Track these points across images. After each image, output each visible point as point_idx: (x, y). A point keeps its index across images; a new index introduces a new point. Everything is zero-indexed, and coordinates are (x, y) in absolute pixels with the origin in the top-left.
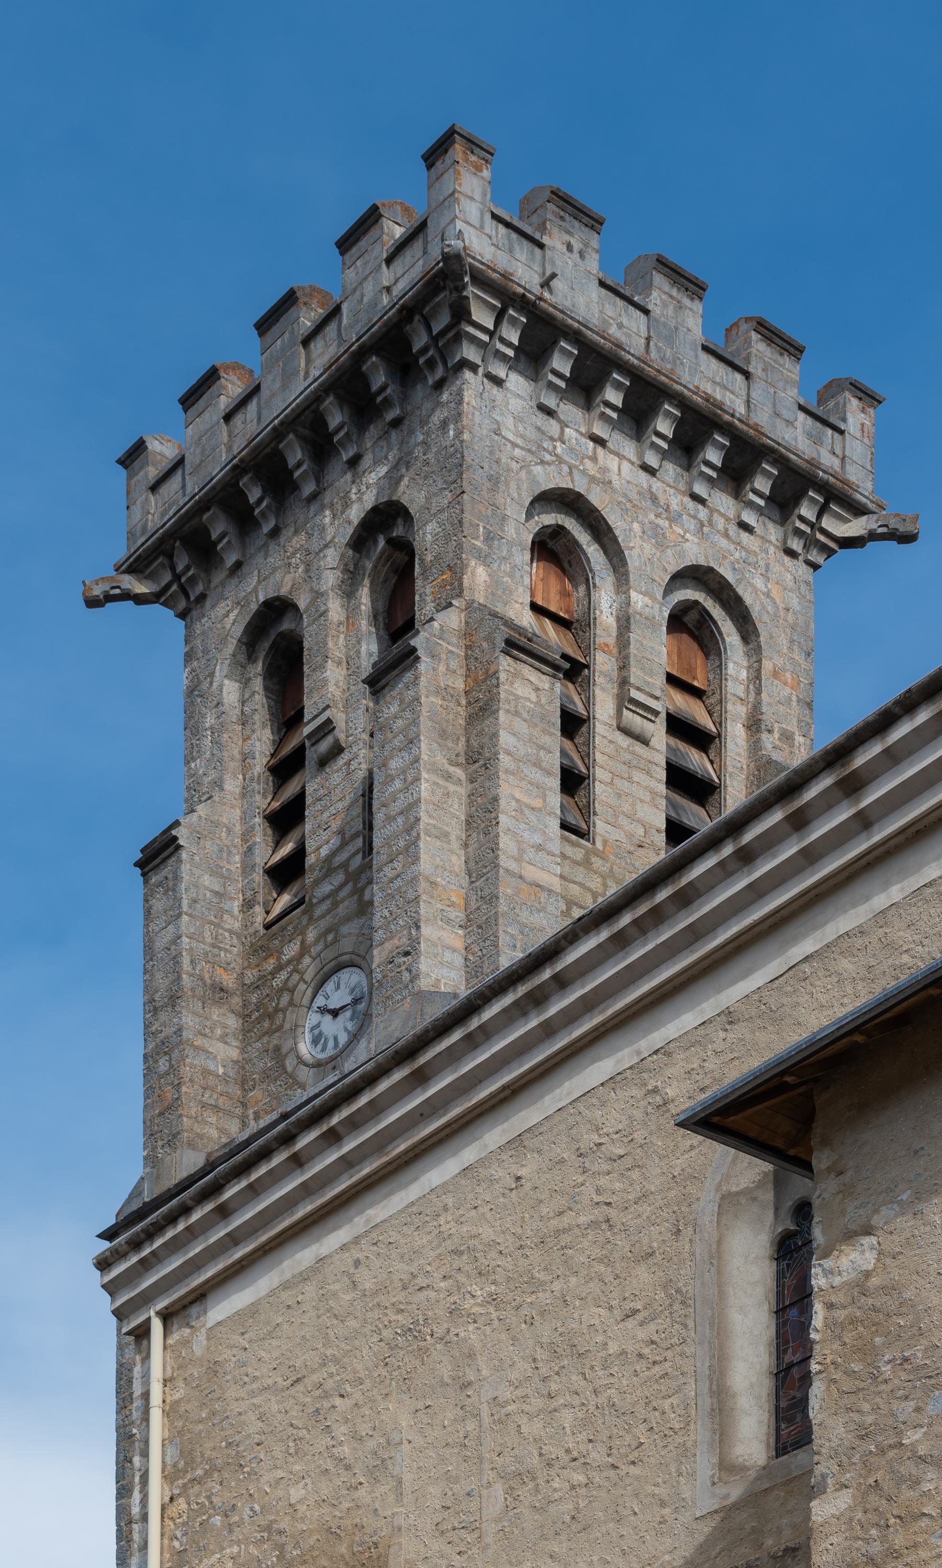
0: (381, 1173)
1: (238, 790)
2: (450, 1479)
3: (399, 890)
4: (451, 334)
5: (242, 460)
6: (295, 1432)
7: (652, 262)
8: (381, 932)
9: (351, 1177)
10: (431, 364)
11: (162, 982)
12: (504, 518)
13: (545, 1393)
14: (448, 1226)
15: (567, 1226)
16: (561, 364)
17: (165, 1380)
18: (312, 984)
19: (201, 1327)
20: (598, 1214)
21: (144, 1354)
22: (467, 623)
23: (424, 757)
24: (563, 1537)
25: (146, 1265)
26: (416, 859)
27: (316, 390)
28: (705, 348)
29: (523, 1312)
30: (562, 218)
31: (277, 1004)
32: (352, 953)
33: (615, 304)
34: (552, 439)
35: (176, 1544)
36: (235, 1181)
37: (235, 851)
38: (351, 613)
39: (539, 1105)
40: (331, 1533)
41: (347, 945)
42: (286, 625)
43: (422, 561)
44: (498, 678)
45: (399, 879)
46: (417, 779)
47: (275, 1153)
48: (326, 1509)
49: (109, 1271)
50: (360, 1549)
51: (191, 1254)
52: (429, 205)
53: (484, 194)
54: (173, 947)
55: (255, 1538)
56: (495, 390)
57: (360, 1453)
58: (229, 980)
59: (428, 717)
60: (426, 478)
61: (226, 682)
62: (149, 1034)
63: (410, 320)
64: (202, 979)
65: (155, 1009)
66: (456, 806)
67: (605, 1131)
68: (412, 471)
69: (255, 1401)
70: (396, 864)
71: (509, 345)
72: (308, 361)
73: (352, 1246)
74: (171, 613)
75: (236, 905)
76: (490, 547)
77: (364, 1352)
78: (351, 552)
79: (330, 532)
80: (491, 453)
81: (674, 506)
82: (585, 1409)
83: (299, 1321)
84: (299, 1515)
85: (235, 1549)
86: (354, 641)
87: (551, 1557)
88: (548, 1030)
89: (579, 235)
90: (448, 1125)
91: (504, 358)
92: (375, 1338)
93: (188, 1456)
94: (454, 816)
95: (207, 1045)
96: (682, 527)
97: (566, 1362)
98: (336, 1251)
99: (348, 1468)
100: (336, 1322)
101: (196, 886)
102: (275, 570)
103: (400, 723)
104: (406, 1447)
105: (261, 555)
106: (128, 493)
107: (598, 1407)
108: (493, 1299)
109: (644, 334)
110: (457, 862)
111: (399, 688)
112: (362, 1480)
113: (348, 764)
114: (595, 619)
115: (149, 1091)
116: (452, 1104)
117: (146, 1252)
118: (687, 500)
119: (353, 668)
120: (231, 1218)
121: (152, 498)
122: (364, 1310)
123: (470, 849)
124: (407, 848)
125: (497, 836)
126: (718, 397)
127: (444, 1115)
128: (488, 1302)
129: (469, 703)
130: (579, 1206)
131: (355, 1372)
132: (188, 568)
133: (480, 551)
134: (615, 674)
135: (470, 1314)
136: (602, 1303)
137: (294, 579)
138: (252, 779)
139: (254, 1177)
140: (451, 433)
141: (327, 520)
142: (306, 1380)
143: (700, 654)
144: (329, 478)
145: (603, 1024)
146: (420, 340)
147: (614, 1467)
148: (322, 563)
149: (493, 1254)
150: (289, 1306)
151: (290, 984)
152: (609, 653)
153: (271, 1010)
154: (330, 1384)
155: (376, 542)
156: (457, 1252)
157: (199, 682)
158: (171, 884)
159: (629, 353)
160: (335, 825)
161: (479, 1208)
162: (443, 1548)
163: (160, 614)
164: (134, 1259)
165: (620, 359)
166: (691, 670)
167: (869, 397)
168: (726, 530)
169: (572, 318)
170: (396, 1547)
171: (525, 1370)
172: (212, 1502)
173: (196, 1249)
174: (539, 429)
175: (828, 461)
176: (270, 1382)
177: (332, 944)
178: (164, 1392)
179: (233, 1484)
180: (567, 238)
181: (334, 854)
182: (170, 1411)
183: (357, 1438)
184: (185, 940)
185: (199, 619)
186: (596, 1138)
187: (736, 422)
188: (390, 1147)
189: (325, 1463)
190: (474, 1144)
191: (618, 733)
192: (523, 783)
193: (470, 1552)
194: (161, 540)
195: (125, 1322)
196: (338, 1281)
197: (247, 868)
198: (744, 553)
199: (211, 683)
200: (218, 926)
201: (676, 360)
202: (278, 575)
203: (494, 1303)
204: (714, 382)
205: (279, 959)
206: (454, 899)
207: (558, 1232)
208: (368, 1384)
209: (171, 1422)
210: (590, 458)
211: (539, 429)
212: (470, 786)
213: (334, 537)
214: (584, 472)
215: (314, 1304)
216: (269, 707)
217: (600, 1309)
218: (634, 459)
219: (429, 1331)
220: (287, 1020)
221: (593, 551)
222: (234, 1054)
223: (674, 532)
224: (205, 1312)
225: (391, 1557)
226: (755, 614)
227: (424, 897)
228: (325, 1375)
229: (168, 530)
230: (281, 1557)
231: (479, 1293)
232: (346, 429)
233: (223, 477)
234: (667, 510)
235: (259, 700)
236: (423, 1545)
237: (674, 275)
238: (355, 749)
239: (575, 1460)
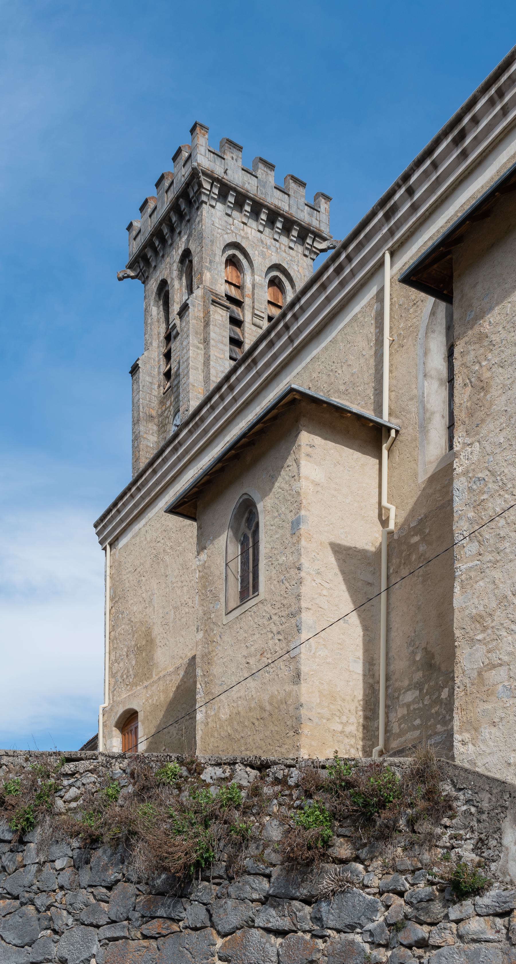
1: (157, 346)
4: (198, 192)
7: (258, 159)
10: (195, 201)
12: (215, 255)
16: (231, 199)
23: (191, 342)
26: (188, 378)
28: (275, 188)
30: (230, 148)
33: (247, 176)
34: (230, 225)
46: (189, 349)
56: (212, 210)
58: (154, 413)
61: (153, 307)
63: (188, 187)
64: (146, 414)
71: (215, 194)
74: (140, 282)
76: (211, 265)
78: (180, 265)
80: (211, 232)
81: (269, 244)
89: (236, 153)
91: (214, 199)
104: (155, 595)
109: (256, 185)
118: (273, 240)
126: (280, 205)
132: (143, 267)
133: (208, 267)
143: (280, 293)
146: (191, 194)
152: (249, 297)
163: (138, 282)
165: (248, 195)
166: (277, 299)
167: (327, 198)
174: (226, 222)
175: (315, 223)
180: (232, 155)
184: (141, 400)
194: (136, 258)
197: (159, 373)
200: (150, 394)
201: (266, 194)
204: (279, 199)
211: (226, 222)
214: (240, 235)
218: (256, 228)
221: (244, 262)
222: (156, 439)
226: (294, 279)
227: (191, 391)
234: (266, 245)
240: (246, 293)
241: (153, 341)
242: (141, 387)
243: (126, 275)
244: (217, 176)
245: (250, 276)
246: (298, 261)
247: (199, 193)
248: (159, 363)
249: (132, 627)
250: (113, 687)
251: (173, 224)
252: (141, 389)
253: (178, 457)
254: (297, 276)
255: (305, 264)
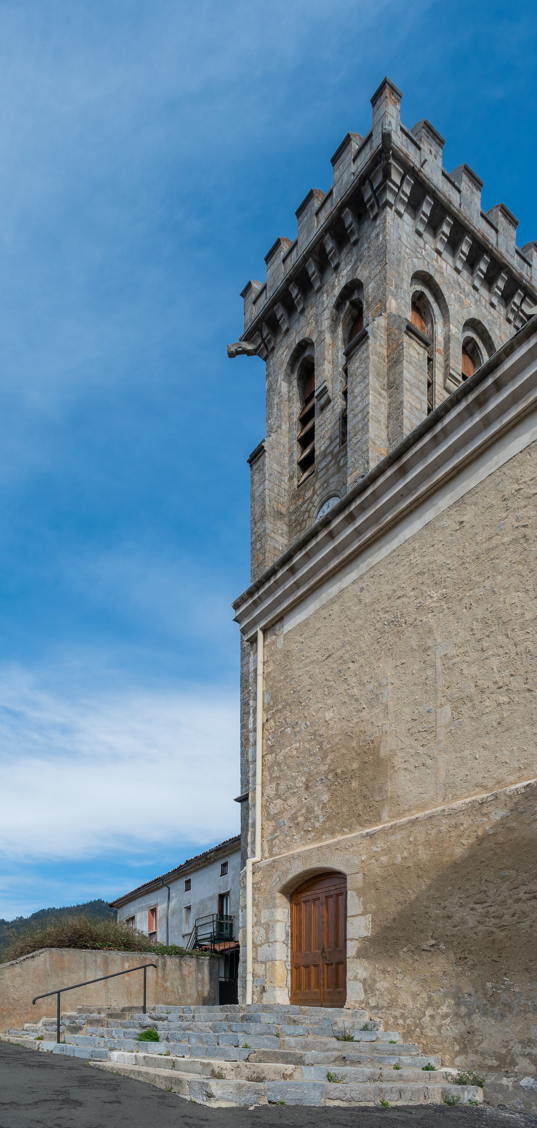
0: (376, 537)
1: (287, 430)
2: (416, 703)
3: (359, 448)
5: (290, 276)
6: (328, 683)
8: (351, 469)
9: (360, 540)
10: (372, 207)
11: (258, 510)
13: (479, 648)
14: (415, 560)
15: (495, 545)
17: (264, 662)
18: (318, 507)
19: (281, 634)
20: (517, 534)
21: (254, 651)
22: (388, 324)
23: (371, 383)
24: (492, 735)
25: (256, 604)
27: (322, 231)
29: (464, 602)
30: (428, 137)
31: (303, 519)
32: (335, 490)
34: (421, 247)
35: (269, 742)
36: (299, 552)
37: (286, 455)
38: (334, 339)
39: (475, 475)
40: (348, 735)
41: (332, 487)
42: (307, 354)
43: (367, 302)
44: (403, 345)
45: (359, 443)
46: (368, 394)
47: (320, 533)
48: (345, 723)
49: (239, 609)
50: (364, 744)
51: (277, 596)
52: (373, 124)
53: (398, 117)
54: (262, 495)
55: (308, 739)
57: (364, 692)
58: (284, 510)
59: (373, 365)
60: (369, 263)
61: (283, 382)
62: (253, 533)
64: (273, 508)
65: (255, 522)
66: (383, 409)
67: (523, 480)
68: (362, 263)
69: (307, 669)
70: (358, 436)
71: (406, 195)
72: (318, 222)
73: (359, 580)
75: (286, 478)
76: (397, 291)
77: (366, 637)
78: (335, 311)
79: (326, 303)
81: (467, 290)
82: (507, 656)
83: (330, 625)
84: (330, 726)
85: (298, 745)
86: (335, 352)
87: (483, 747)
88: (486, 423)
89: (435, 148)
90: (417, 499)
92: (372, 628)
93: (274, 698)
94: (382, 413)
95: (275, 537)
96: (469, 300)
97: (494, 629)
98: (350, 585)
99: (357, 700)
100: (350, 623)
101: (271, 468)
102: (302, 328)
103: (360, 370)
104: (390, 687)
105: (297, 323)
106: (245, 308)
107: (517, 654)
108: (445, 597)
109: (459, 202)
110: (384, 435)
111: (360, 354)
112: (364, 706)
113: (333, 407)
114: (435, 337)
115: (253, 557)
116: (421, 485)
117: (256, 597)
118: (471, 288)
119: (335, 364)
120: (296, 573)
121: (254, 308)
122: (366, 614)
123: (389, 429)
124: (363, 427)
125: (402, 420)
127: (415, 493)
128: (441, 599)
129: (389, 361)
130: (504, 532)
131: (360, 648)
132: (268, 335)
133: (393, 292)
134: (443, 364)
135: (429, 608)
136: (519, 589)
137: (311, 329)
138: (293, 424)
139: (308, 548)
140: (381, 238)
141: (325, 298)
142: (334, 655)
143: (472, 366)
144: (325, 279)
145: (524, 410)
146: (368, 194)
147: (529, 690)
148: (323, 318)
149: (445, 571)
150: (325, 618)
151: (308, 509)
153: (300, 521)
154: (347, 656)
155: (345, 304)
156: (421, 573)
157: (272, 385)
158: (261, 468)
159: (454, 206)
160: (327, 436)
161: (435, 546)
162: (412, 743)
164: (250, 601)
165: (450, 209)
168: (486, 305)
169: (432, 184)
170: (384, 742)
171: (466, 636)
172: (286, 721)
173: (279, 592)
176: (315, 658)
177: (326, 488)
178: (264, 668)
179: (296, 712)
180: (430, 147)
181: (327, 448)
182: (267, 677)
183: (362, 684)
184: (267, 491)
185: (272, 359)
186: (517, 487)
187: (494, 250)
188: (383, 519)
189: (344, 698)
190: (432, 509)
191: (444, 390)
192: (413, 396)
193: (429, 745)
194: (258, 323)
195: (246, 635)
196: (351, 600)
197: (291, 462)
198: (492, 318)
199: (277, 385)
200: (279, 486)
202: (304, 330)
203: (445, 599)
205: (304, 498)
206: (382, 452)
207: (488, 550)
208: (368, 654)
209: (267, 683)
210: (435, 260)
211: (416, 242)
212: (389, 400)
213: (328, 305)
214: (433, 266)
215: (338, 615)
216: (299, 393)
217: (518, 593)
218: (452, 265)
219: (404, 621)
220: (307, 524)
222: (286, 542)
223: (466, 301)
224: (283, 627)
225: (381, 748)
227: (371, 449)
228: (344, 652)
229: (260, 317)
230: (321, 749)
231: (435, 595)
232: (334, 251)
233: (282, 286)
234: (464, 291)
235: (296, 390)
236: (400, 741)
237: (471, 177)
238: (336, 400)
239: (500, 688)
240: (437, 347)
241: (283, 423)
242: (267, 475)
243: (240, 349)
244: (412, 165)
245: (442, 327)
246: (500, 325)
247: (383, 188)
248: (290, 451)
249: (321, 744)
250: (272, 834)
251: (328, 255)
252: (267, 477)
253: (356, 530)
254: (499, 343)
255: (508, 332)
